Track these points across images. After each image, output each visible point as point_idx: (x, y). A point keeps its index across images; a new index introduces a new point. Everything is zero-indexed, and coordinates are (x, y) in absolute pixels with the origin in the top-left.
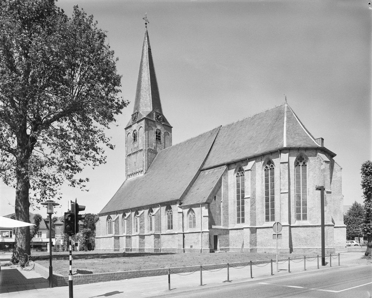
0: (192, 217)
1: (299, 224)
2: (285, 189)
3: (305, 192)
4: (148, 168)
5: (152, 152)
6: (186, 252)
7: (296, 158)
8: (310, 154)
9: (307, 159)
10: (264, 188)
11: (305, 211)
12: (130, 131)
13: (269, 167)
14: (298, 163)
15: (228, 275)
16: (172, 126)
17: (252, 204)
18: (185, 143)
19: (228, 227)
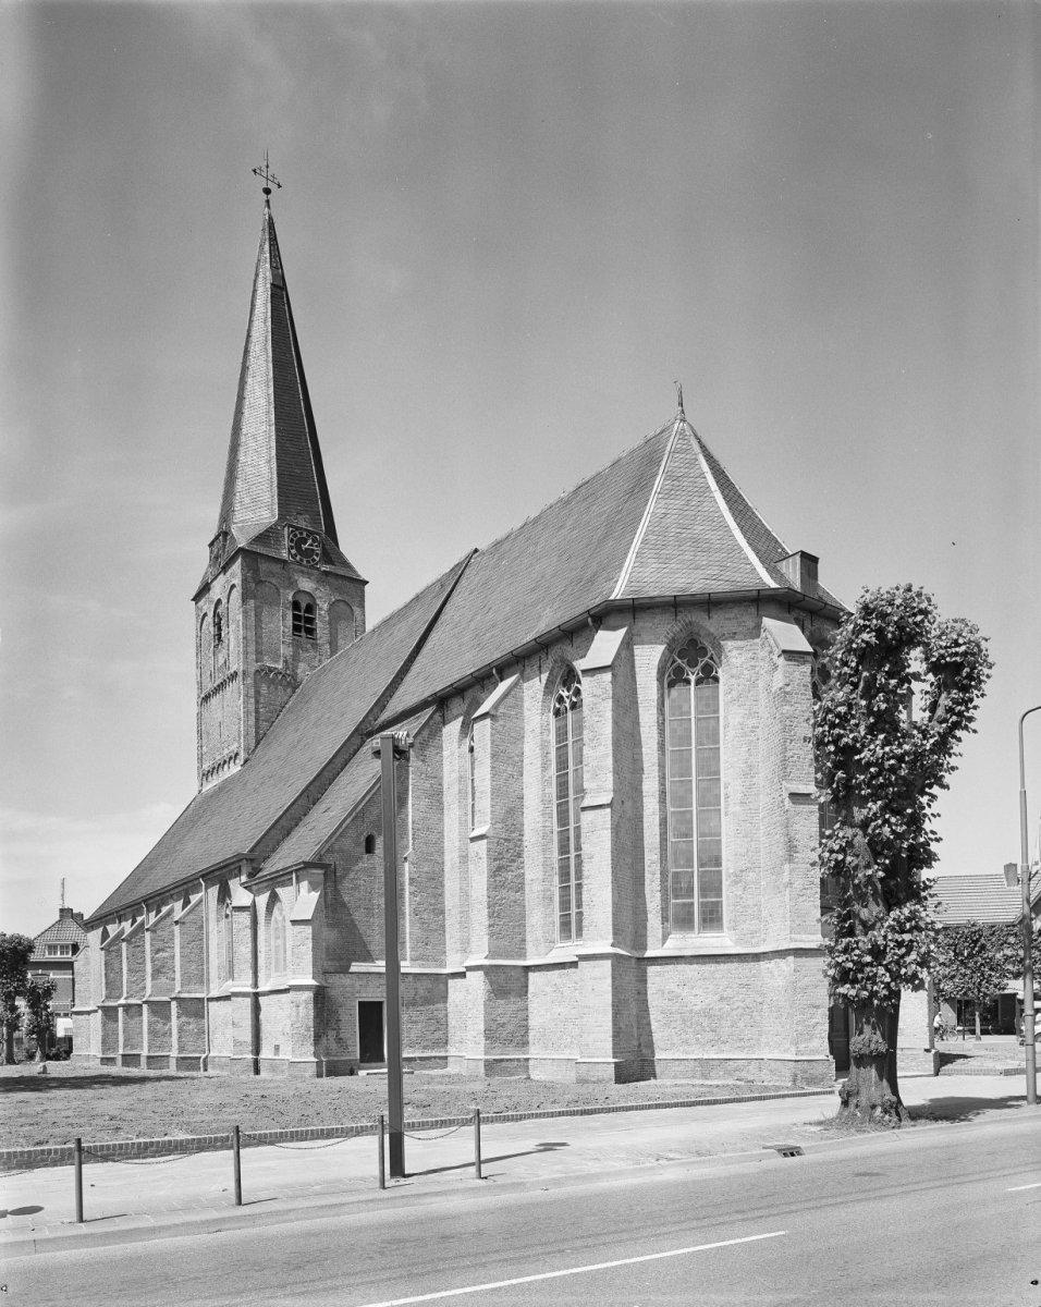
1: (680, 949)
2: (599, 789)
3: (711, 800)
4: (258, 743)
5: (272, 681)
6: (264, 1074)
7: (670, 649)
8: (731, 626)
9: (719, 649)
10: (553, 790)
11: (712, 886)
12: (207, 606)
13: (568, 697)
14: (679, 671)
16: (364, 576)
17: (502, 862)
19: (445, 967)
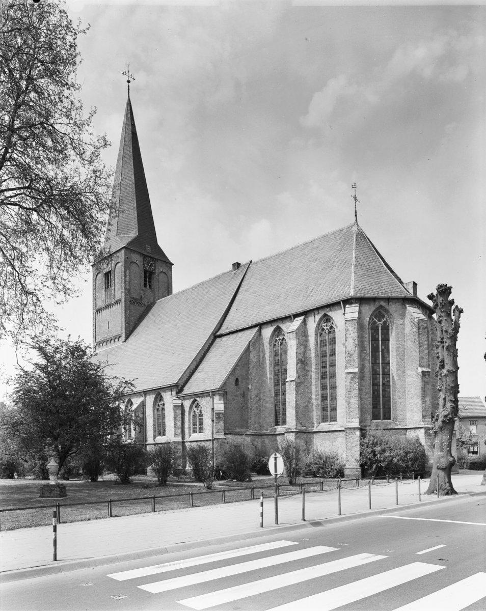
0: (197, 414)
15: (397, 498)
16: (172, 261)
18: (193, 289)
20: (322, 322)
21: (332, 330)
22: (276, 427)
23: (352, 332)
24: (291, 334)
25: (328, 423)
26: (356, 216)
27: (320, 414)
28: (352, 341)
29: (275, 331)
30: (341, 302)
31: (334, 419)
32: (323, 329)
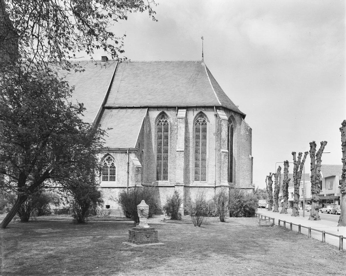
20: (198, 116)
21: (204, 123)
22: (157, 181)
23: (225, 127)
24: (181, 119)
25: (199, 182)
26: (203, 56)
27: (194, 175)
28: (225, 133)
29: (160, 114)
30: (214, 107)
31: (204, 179)
32: (198, 121)
